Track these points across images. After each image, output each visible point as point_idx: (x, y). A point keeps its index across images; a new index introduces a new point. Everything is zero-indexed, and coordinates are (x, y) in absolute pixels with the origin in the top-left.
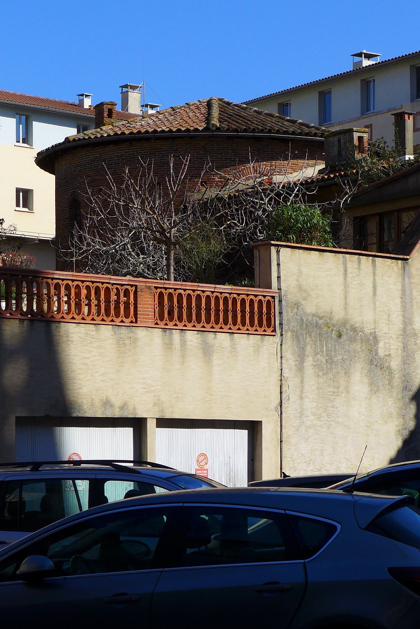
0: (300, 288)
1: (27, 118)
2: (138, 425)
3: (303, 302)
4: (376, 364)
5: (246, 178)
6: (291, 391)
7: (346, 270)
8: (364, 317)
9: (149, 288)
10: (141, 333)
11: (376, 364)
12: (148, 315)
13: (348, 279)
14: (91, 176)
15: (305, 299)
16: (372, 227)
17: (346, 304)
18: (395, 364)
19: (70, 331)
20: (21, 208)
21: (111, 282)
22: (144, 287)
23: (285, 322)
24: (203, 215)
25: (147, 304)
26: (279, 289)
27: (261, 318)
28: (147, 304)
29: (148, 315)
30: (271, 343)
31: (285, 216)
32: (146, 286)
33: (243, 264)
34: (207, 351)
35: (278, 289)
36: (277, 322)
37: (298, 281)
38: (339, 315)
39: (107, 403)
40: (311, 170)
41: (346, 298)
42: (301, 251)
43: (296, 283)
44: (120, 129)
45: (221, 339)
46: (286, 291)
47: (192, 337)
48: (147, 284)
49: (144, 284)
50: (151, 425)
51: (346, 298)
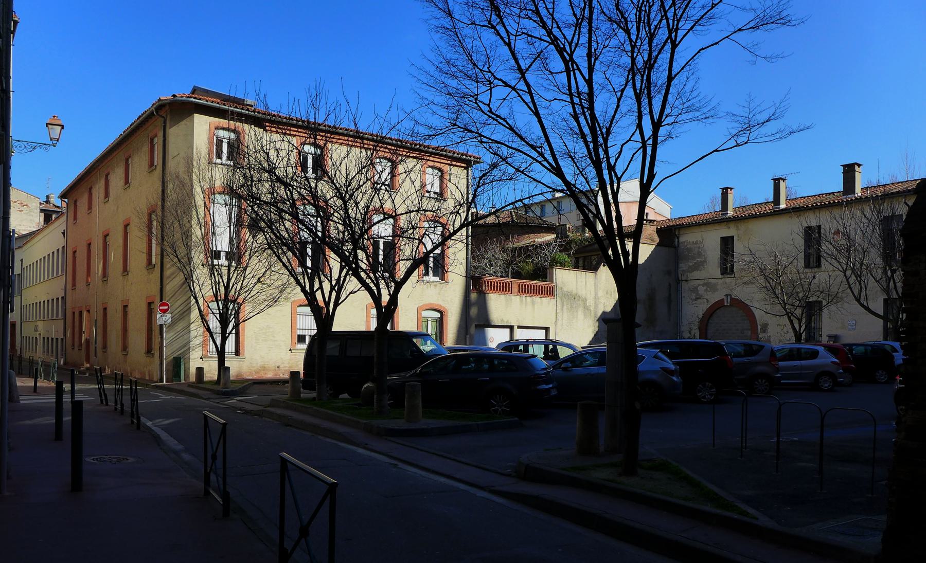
2: (511, 328)
4: (586, 308)
5: (527, 240)
6: (559, 315)
8: (582, 293)
10: (513, 297)
11: (586, 308)
16: (581, 262)
18: (592, 309)
25: (515, 288)
27: (550, 292)
28: (515, 288)
30: (553, 300)
31: (895, 296)
33: (542, 273)
34: (533, 303)
38: (574, 292)
39: (502, 320)
40: (550, 237)
45: (538, 299)
47: (529, 299)
50: (516, 328)
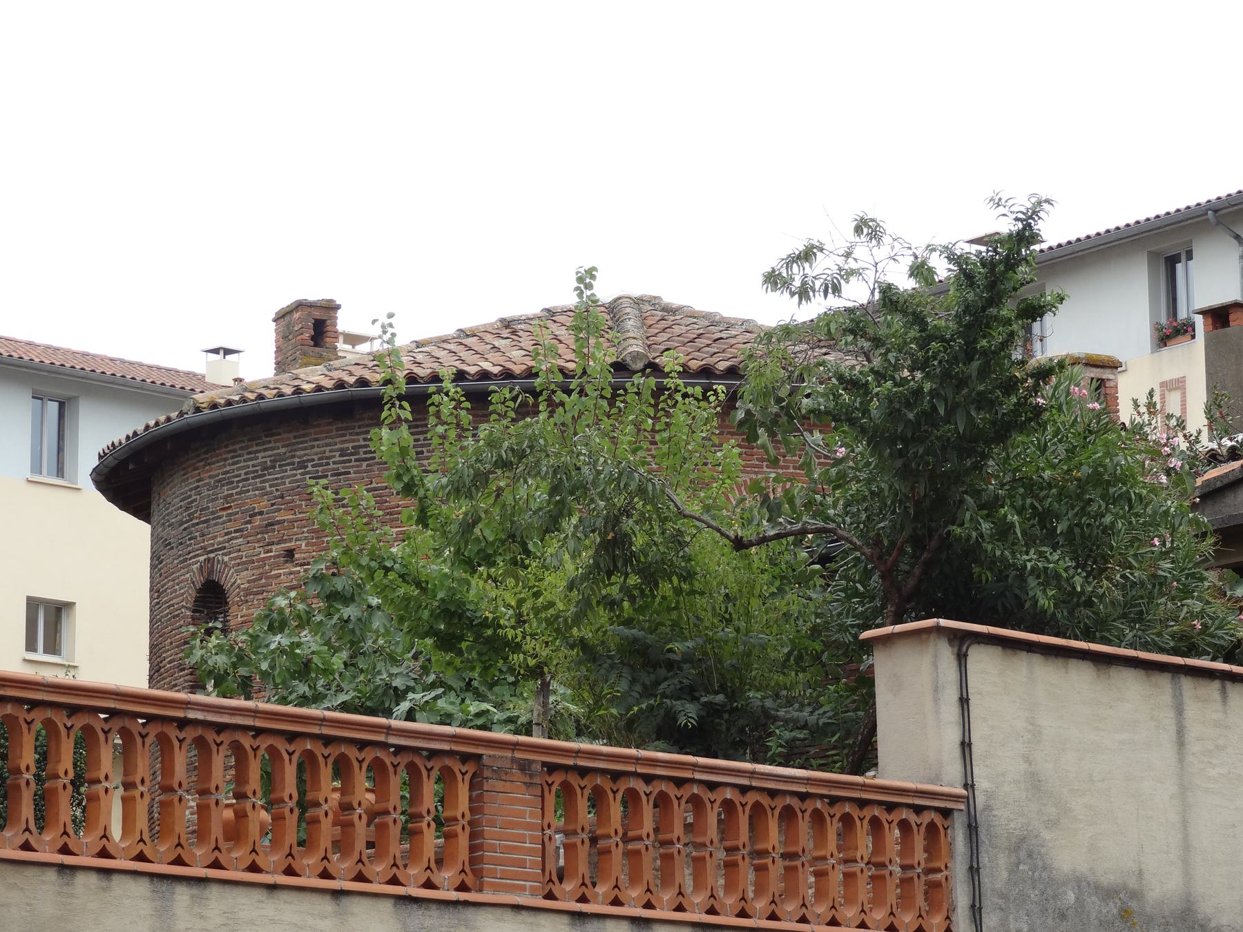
0: (1035, 782)
1: (62, 406)
3: (1047, 835)
7: (1181, 731)
9: (524, 766)
12: (522, 864)
13: (1190, 758)
14: (261, 513)
15: (1052, 824)
17: (1186, 847)
19: (865, 302)
20: (40, 656)
21: (393, 740)
22: (507, 764)
23: (989, 901)
24: (681, 554)
26: (969, 786)
29: (522, 864)
32: (513, 760)
35: (966, 786)
36: (962, 899)
37: (1028, 760)
41: (1185, 824)
42: (1037, 659)
43: (1023, 766)
44: (351, 374)
46: (990, 795)
48: (518, 755)
49: (509, 754)
51: (1185, 824)
